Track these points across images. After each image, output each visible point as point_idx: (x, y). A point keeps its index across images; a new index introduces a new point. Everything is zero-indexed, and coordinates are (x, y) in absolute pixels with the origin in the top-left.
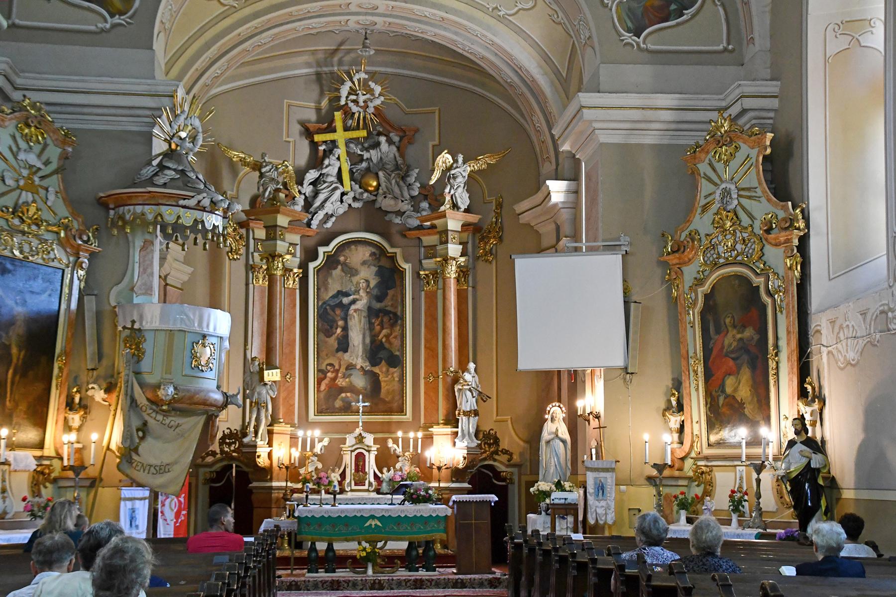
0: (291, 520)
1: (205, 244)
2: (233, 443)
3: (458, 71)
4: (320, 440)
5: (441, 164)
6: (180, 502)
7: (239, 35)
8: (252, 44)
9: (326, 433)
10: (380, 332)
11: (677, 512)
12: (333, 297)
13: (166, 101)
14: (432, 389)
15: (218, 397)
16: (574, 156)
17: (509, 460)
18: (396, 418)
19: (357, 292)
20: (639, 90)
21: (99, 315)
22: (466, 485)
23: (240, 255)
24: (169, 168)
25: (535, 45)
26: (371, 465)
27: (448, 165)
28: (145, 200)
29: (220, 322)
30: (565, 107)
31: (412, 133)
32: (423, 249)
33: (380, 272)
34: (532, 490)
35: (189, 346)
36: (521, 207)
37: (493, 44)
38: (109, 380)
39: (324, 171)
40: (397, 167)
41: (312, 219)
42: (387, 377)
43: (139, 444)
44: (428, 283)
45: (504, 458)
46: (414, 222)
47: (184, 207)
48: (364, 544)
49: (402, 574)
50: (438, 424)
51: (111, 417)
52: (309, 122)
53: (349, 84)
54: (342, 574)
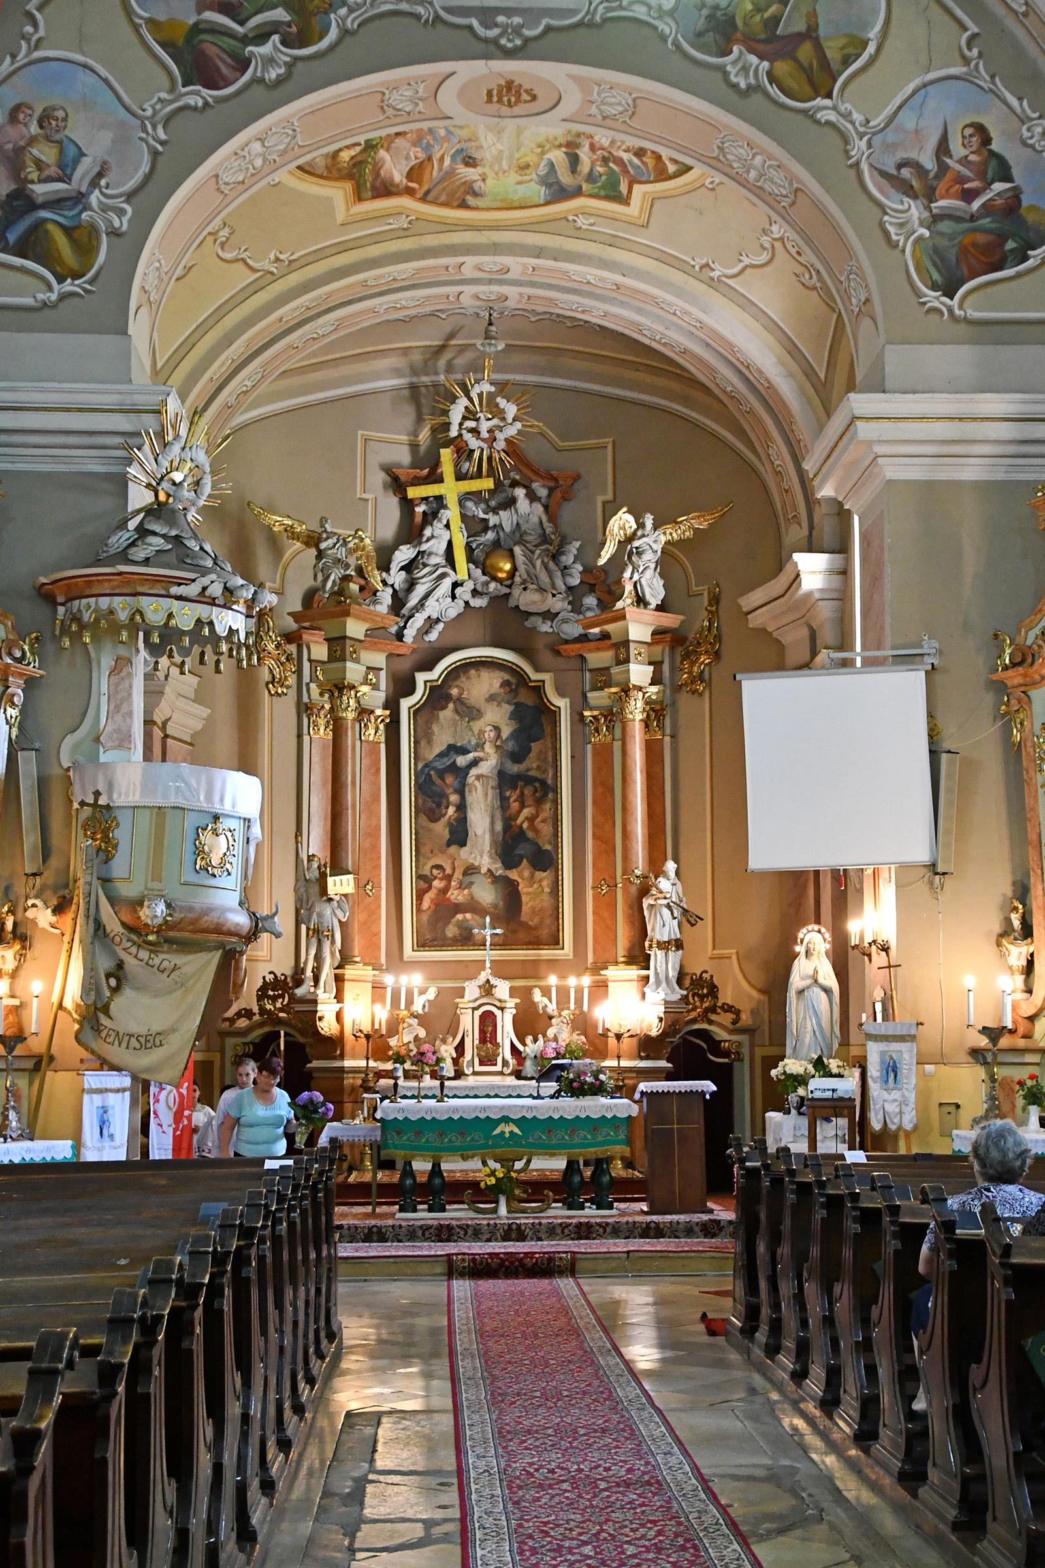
0: (370, 1125)
1: (218, 662)
2: (279, 996)
3: (642, 376)
4: (423, 992)
5: (616, 530)
6: (181, 1094)
7: (281, 320)
8: (301, 336)
9: (432, 978)
10: (520, 812)
11: (1024, 1109)
12: (441, 755)
13: (149, 419)
14: (606, 904)
15: (241, 920)
16: (841, 504)
17: (734, 1022)
18: (546, 953)
19: (480, 746)
20: (954, 387)
21: (43, 784)
22: (663, 1064)
23: (288, 687)
24: (154, 533)
25: (773, 327)
26: (506, 1031)
27: (629, 532)
28: (113, 589)
29: (241, 793)
30: (821, 427)
31: (569, 482)
32: (588, 674)
33: (518, 714)
34: (773, 1073)
35: (190, 835)
36: (749, 601)
37: (703, 326)
38: (61, 893)
39: (424, 547)
40: (544, 539)
41: (405, 627)
42: (532, 889)
43: (111, 999)
44: (597, 730)
45: (726, 1018)
46: (573, 630)
47: (179, 598)
48: (493, 1164)
49: (557, 1212)
50: (616, 963)
51: (64, 955)
52: (399, 466)
53: (463, 402)
54: (456, 1213)
